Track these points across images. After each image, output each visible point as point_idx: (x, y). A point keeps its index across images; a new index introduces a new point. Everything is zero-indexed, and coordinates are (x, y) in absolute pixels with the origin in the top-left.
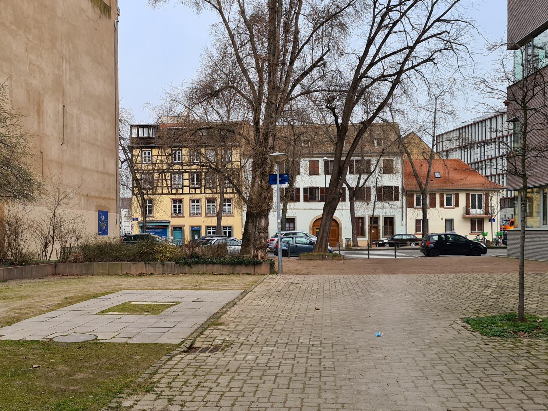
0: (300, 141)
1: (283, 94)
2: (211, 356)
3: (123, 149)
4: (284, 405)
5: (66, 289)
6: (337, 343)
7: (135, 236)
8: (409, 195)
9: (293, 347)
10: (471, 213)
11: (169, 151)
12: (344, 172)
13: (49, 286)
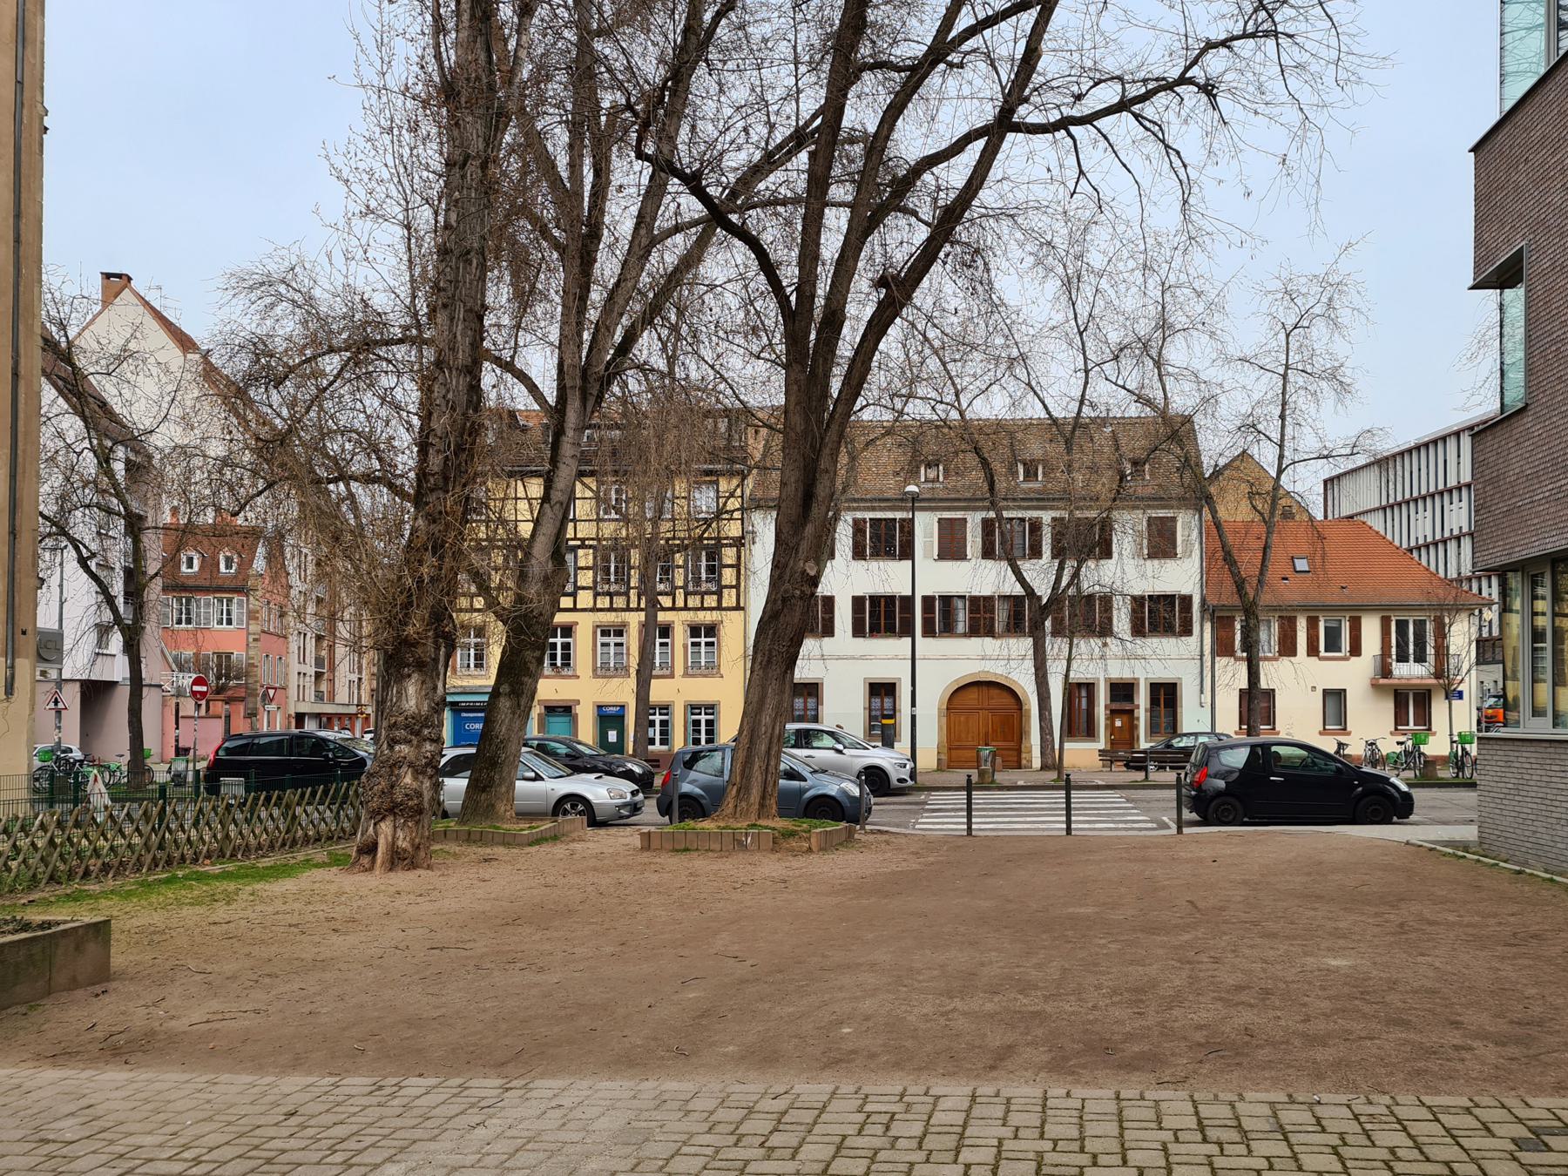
8: (1220, 620)
10: (1396, 672)
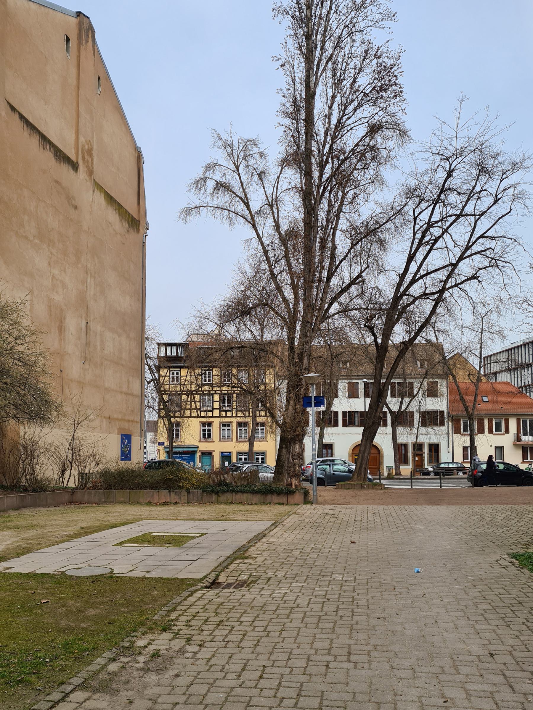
0: (338, 361)
1: (319, 312)
2: (235, 592)
3: (150, 368)
4: (312, 646)
5: (83, 519)
6: (372, 580)
7: (160, 462)
8: (456, 421)
9: (324, 584)
10: (523, 440)
11: (198, 371)
12: (384, 394)
13: (65, 515)
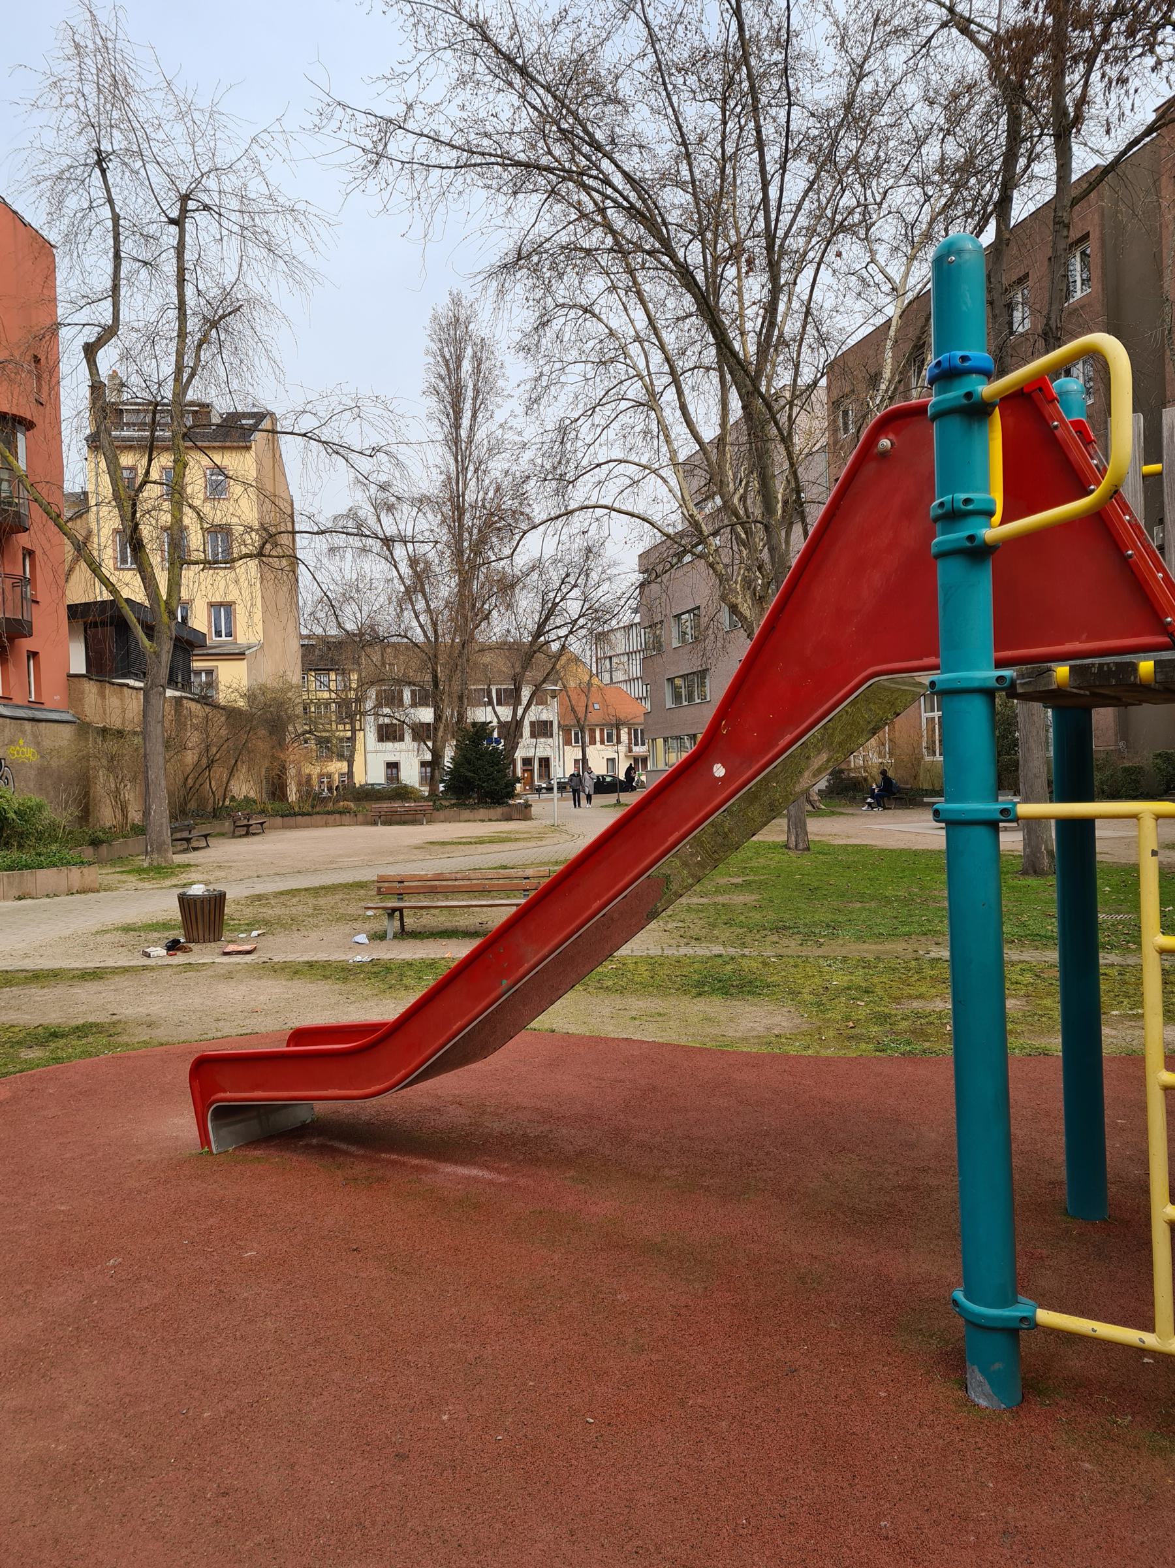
8: (565, 729)
